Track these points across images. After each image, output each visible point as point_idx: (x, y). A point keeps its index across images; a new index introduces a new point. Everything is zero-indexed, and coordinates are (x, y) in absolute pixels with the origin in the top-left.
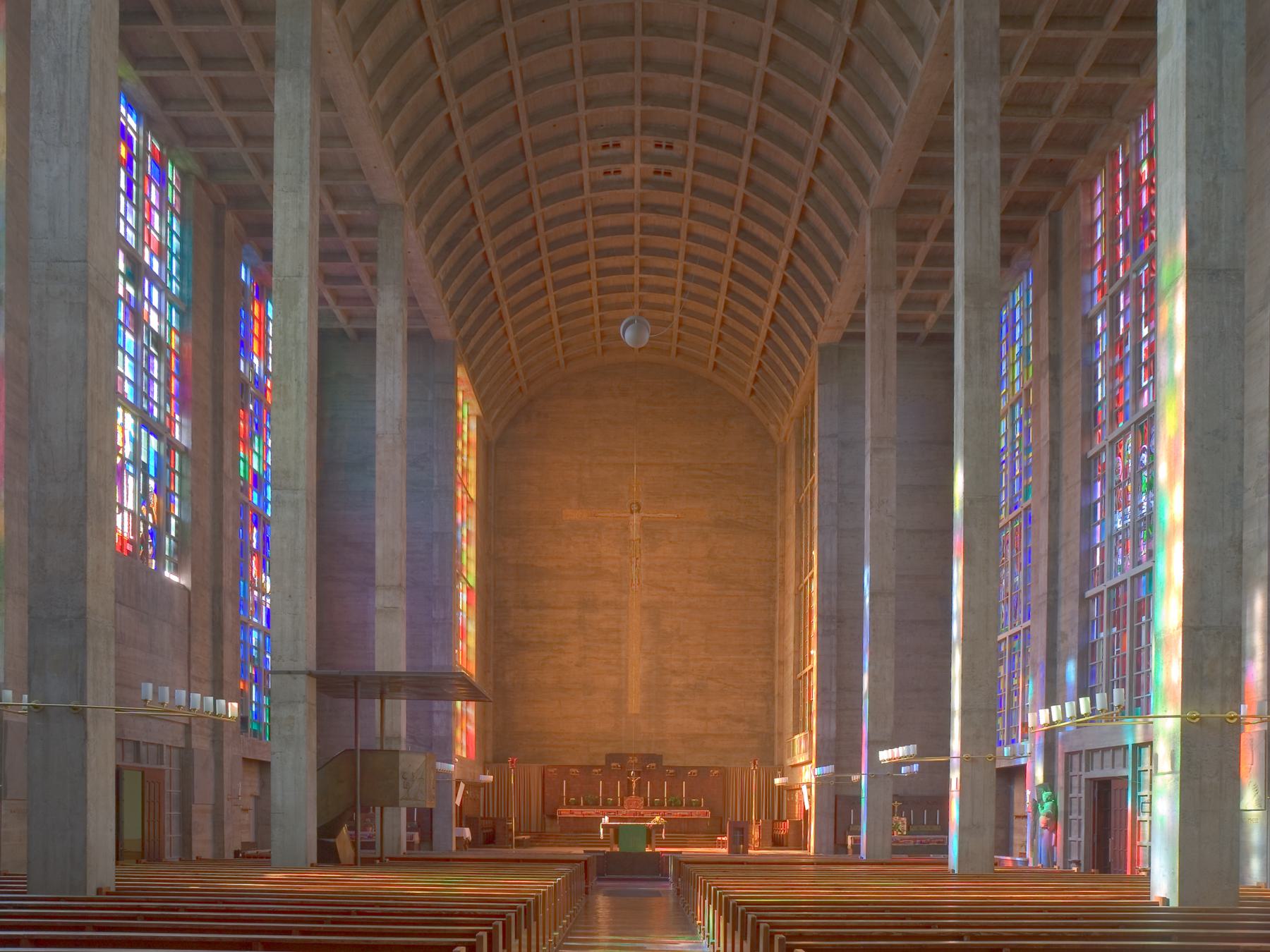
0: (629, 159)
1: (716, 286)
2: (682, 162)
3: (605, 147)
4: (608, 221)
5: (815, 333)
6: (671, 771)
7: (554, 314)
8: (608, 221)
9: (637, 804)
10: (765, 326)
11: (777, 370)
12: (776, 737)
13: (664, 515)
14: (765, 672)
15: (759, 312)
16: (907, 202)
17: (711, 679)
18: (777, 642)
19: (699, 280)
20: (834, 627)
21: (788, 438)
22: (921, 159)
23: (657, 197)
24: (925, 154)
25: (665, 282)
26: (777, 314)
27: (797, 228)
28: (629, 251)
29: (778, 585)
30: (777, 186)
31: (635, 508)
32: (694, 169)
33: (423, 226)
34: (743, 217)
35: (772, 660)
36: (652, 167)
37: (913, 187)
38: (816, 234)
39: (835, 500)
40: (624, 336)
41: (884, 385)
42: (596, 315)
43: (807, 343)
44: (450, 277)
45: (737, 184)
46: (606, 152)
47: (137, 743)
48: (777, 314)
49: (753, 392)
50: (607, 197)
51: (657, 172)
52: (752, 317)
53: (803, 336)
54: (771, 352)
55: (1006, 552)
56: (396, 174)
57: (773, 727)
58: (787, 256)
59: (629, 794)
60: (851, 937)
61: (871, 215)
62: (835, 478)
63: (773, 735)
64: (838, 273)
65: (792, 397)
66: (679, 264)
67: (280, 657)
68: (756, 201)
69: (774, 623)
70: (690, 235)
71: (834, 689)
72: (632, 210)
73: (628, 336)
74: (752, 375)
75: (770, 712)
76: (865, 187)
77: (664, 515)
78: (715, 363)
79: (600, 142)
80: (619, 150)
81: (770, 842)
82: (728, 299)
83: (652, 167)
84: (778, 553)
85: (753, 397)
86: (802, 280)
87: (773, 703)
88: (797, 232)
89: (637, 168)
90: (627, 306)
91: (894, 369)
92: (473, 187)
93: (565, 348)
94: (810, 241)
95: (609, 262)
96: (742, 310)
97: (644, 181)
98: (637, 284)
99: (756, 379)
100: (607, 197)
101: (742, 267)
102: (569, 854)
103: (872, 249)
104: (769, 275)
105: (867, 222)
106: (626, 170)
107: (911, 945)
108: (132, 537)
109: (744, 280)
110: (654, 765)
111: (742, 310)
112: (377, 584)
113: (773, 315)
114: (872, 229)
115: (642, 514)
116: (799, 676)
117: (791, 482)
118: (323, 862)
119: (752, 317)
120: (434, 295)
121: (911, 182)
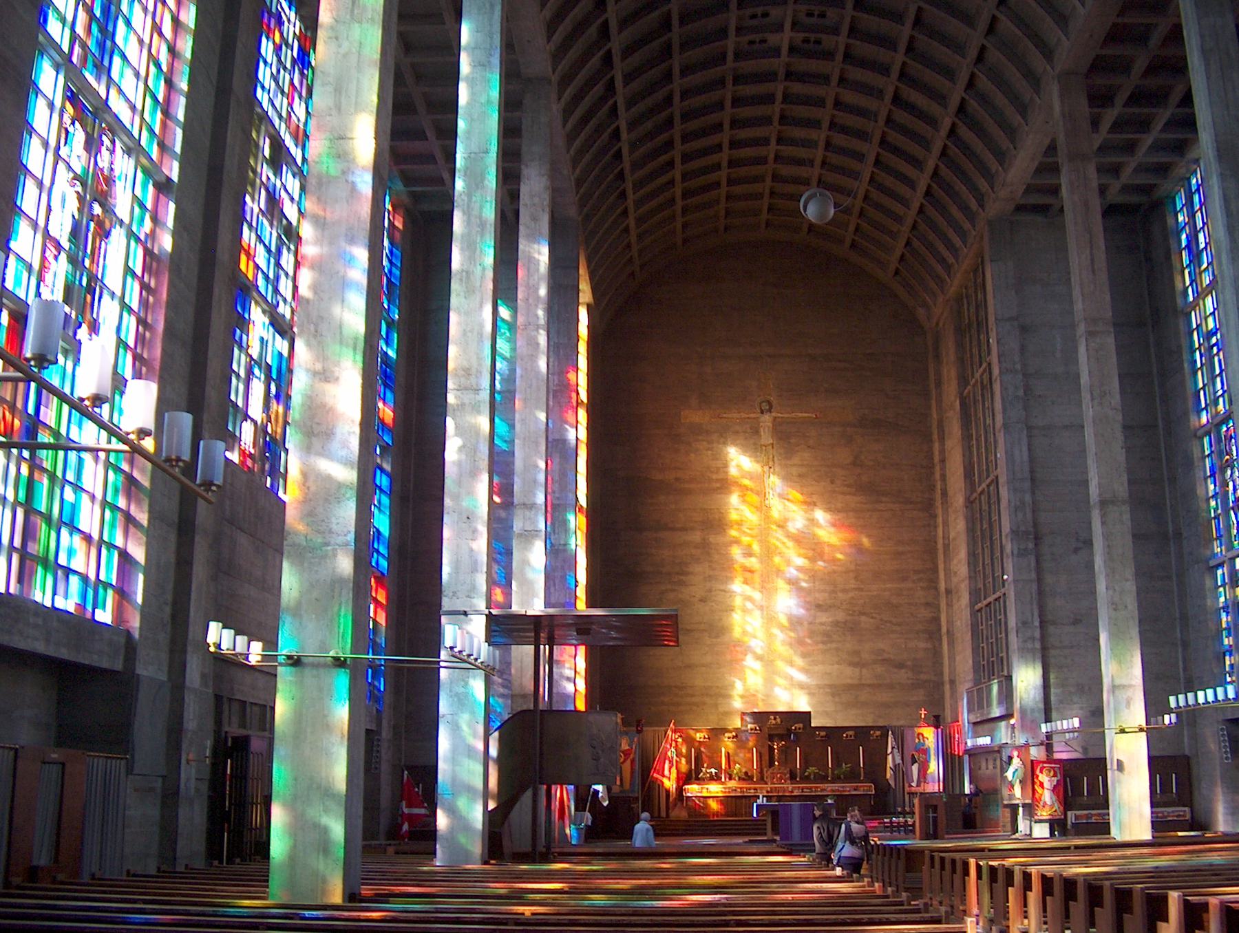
0: (780, 28)
1: (860, 157)
2: (835, 31)
3: (754, 16)
4: (748, 90)
5: (982, 206)
6: (823, 734)
7: (678, 190)
8: (748, 90)
9: (781, 778)
10: (917, 199)
11: (930, 247)
12: (947, 687)
13: (800, 415)
14: (927, 604)
15: (911, 184)
16: (1098, 65)
17: (864, 614)
18: (941, 566)
19: (842, 151)
20: (1031, 545)
21: (941, 325)
22: (1115, 25)
23: (803, 65)
24: (1120, 20)
25: (802, 153)
26: (934, 185)
27: (964, 95)
28: (767, 121)
29: (938, 495)
30: (941, 52)
31: (765, 406)
32: (848, 37)
33: (563, 100)
34: (900, 85)
35: (936, 589)
36: (801, 35)
37: (1104, 52)
38: (984, 100)
39: (1021, 393)
40: (805, 211)
41: (1092, 260)
42: (724, 190)
43: (972, 217)
44: (581, 152)
45: (895, 51)
46: (755, 22)
47: (243, 703)
48: (934, 185)
49: (897, 272)
50: (749, 66)
51: (806, 41)
52: (902, 189)
53: (965, 208)
54: (922, 226)
55: (1231, 449)
56: (548, 48)
57: (942, 674)
58: (950, 125)
59: (771, 764)
60: (69, 919)
61: (1059, 82)
62: (1018, 367)
63: (943, 684)
64: (1013, 140)
65: (949, 277)
66: (820, 136)
67: (454, 593)
68: (916, 68)
69: (936, 542)
70: (838, 104)
71: (1037, 623)
72: (828, 84)
73: (811, 212)
74: (898, 253)
75: (936, 653)
76: (1048, 54)
77: (800, 415)
78: (853, 240)
79: (749, 12)
80: (767, 20)
81: (960, 823)
82: (875, 170)
83: (801, 35)
84: (937, 459)
85: (898, 278)
86: (966, 149)
87: (941, 644)
88: (963, 99)
89: (784, 39)
90: (806, 183)
91: (1101, 243)
92: (616, 59)
93: (685, 226)
94: (979, 108)
95: (743, 134)
96: (889, 181)
97: (792, 50)
98: (772, 156)
99: (902, 258)
100: (749, 66)
101: (895, 137)
102: (694, 845)
103: (1064, 115)
104: (926, 144)
105: (1055, 89)
106: (773, 39)
107: (71, 927)
108: (253, 451)
109: (896, 151)
110: (801, 725)
111: (889, 181)
112: (516, 501)
113: (929, 187)
114: (1061, 96)
115: (774, 414)
116: (977, 607)
117: (950, 373)
118: (1065, 886)
119: (902, 189)
120: (565, 172)
121: (1102, 48)
